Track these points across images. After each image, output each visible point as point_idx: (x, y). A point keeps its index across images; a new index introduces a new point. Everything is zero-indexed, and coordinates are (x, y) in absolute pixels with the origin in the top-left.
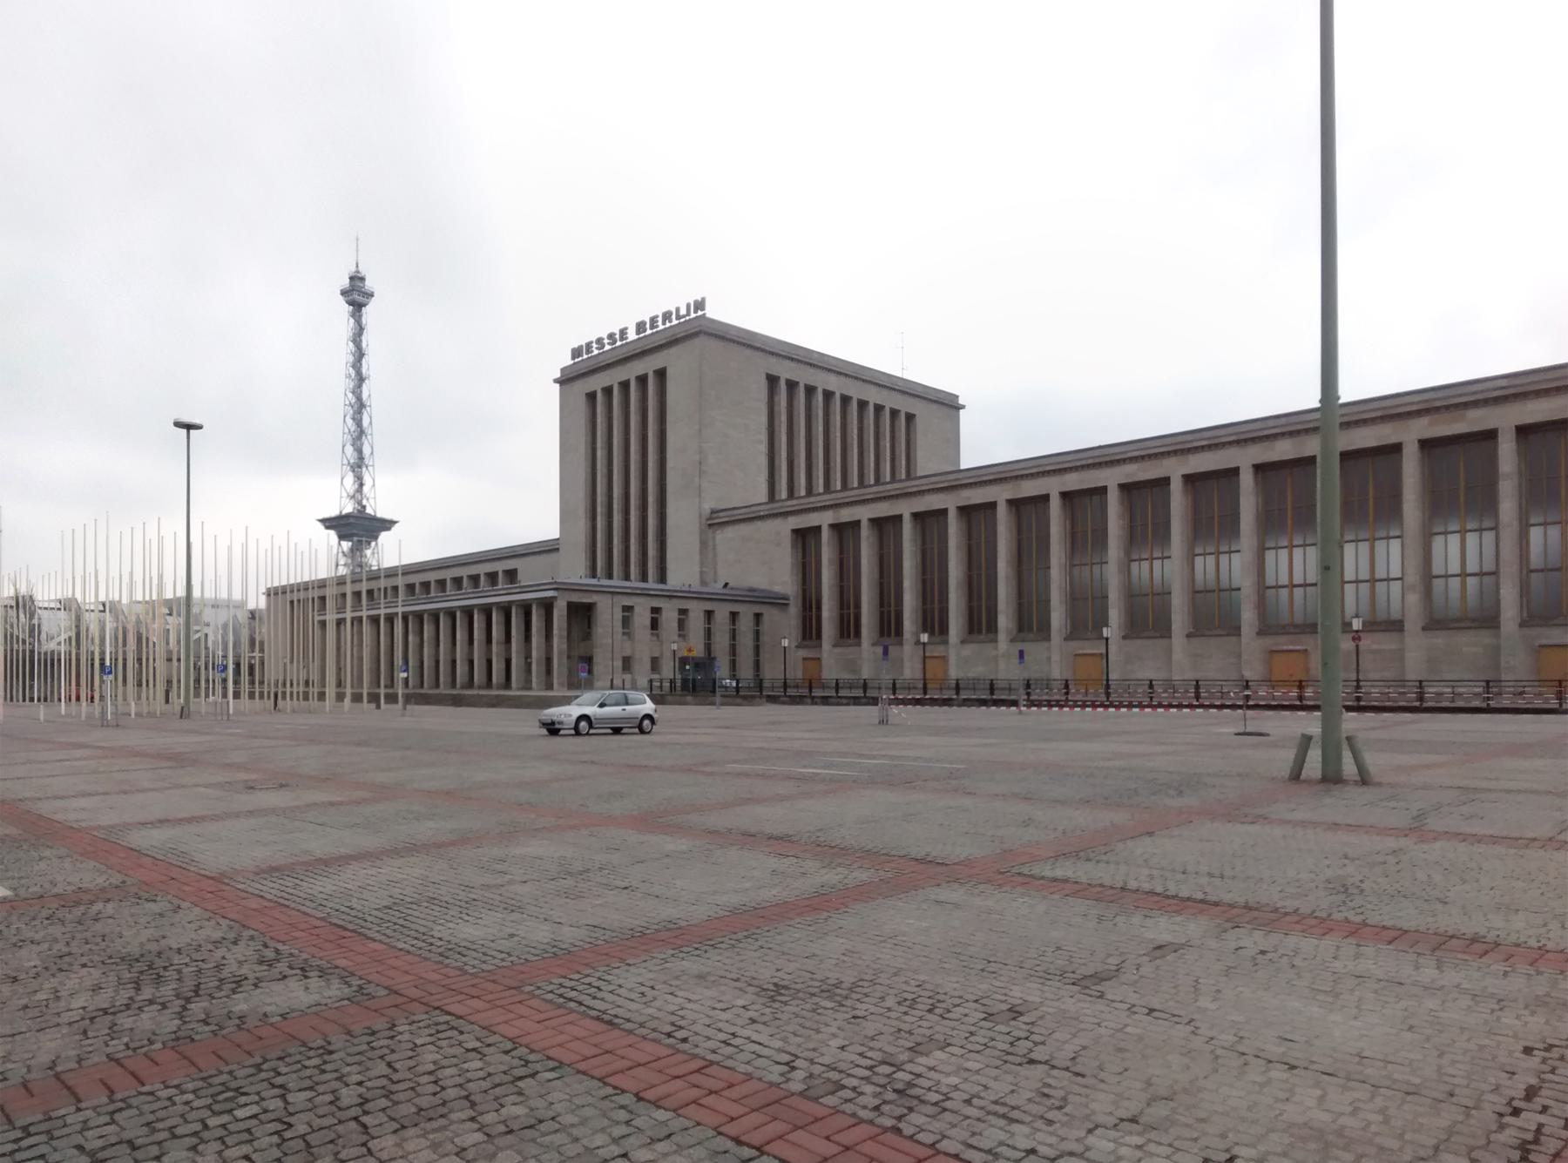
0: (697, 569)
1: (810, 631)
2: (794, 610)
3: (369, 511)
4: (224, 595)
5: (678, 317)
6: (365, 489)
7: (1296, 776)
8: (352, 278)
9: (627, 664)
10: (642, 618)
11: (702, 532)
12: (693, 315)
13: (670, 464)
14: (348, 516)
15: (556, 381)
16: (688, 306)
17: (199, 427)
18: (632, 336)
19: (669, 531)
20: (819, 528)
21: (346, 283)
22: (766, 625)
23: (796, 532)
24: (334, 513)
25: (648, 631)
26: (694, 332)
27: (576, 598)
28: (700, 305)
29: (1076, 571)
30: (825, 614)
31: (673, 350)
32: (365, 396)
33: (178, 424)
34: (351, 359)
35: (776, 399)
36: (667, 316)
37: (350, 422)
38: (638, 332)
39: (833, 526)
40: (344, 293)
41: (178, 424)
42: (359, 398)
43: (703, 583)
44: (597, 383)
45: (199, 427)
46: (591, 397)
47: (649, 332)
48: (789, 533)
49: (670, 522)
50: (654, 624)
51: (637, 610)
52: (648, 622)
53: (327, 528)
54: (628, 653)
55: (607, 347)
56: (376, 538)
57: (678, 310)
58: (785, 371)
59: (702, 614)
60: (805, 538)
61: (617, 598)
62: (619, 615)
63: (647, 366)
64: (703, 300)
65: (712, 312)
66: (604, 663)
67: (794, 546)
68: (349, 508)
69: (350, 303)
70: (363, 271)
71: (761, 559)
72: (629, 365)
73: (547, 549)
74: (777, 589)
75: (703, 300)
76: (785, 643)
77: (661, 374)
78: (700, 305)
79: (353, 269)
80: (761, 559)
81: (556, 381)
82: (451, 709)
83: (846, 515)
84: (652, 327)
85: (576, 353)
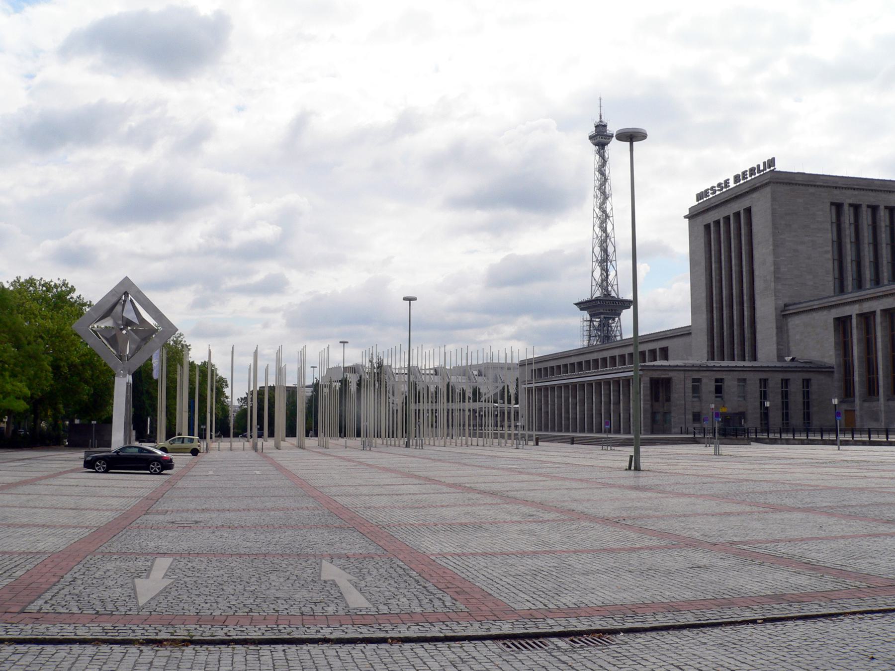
0: (775, 347)
1: (848, 392)
2: (838, 375)
3: (613, 294)
4: (509, 361)
5: (759, 171)
6: (610, 278)
7: (630, 468)
8: (596, 127)
9: (697, 417)
10: (708, 386)
11: (777, 321)
12: (768, 170)
13: (756, 273)
14: (597, 299)
15: (686, 217)
16: (764, 163)
17: (415, 299)
18: (732, 185)
19: (757, 320)
20: (851, 316)
21: (592, 130)
22: (814, 387)
23: (837, 320)
24: (587, 297)
25: (713, 395)
26: (769, 182)
27: (656, 375)
28: (772, 162)
29: (368, 423)
30: (856, 378)
31: (755, 195)
32: (608, 210)
33: (405, 299)
34: (597, 184)
35: (842, 219)
36: (752, 171)
37: (597, 230)
38: (735, 182)
39: (859, 315)
40: (591, 138)
41: (405, 299)
42: (604, 212)
43: (780, 358)
44: (711, 217)
45: (415, 299)
46: (707, 227)
47: (742, 182)
48: (831, 321)
49: (758, 314)
50: (719, 390)
51: (704, 381)
52: (713, 389)
53: (581, 309)
54: (696, 410)
55: (718, 193)
56: (620, 314)
57: (759, 166)
58: (848, 198)
59: (758, 382)
60: (842, 323)
61: (688, 374)
62: (689, 385)
63: (738, 206)
64: (773, 159)
65: (779, 167)
66: (676, 417)
67: (836, 330)
68: (598, 294)
69: (596, 145)
70: (605, 120)
71: (815, 342)
72: (729, 206)
73: (683, 333)
74: (826, 360)
75: (773, 159)
76: (835, 401)
77: (748, 211)
78: (772, 162)
79: (598, 120)
80: (815, 342)
81: (686, 217)
82: (569, 446)
83: (867, 307)
84: (744, 178)
85: (700, 196)
